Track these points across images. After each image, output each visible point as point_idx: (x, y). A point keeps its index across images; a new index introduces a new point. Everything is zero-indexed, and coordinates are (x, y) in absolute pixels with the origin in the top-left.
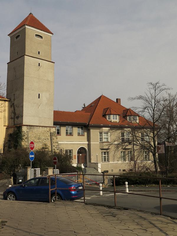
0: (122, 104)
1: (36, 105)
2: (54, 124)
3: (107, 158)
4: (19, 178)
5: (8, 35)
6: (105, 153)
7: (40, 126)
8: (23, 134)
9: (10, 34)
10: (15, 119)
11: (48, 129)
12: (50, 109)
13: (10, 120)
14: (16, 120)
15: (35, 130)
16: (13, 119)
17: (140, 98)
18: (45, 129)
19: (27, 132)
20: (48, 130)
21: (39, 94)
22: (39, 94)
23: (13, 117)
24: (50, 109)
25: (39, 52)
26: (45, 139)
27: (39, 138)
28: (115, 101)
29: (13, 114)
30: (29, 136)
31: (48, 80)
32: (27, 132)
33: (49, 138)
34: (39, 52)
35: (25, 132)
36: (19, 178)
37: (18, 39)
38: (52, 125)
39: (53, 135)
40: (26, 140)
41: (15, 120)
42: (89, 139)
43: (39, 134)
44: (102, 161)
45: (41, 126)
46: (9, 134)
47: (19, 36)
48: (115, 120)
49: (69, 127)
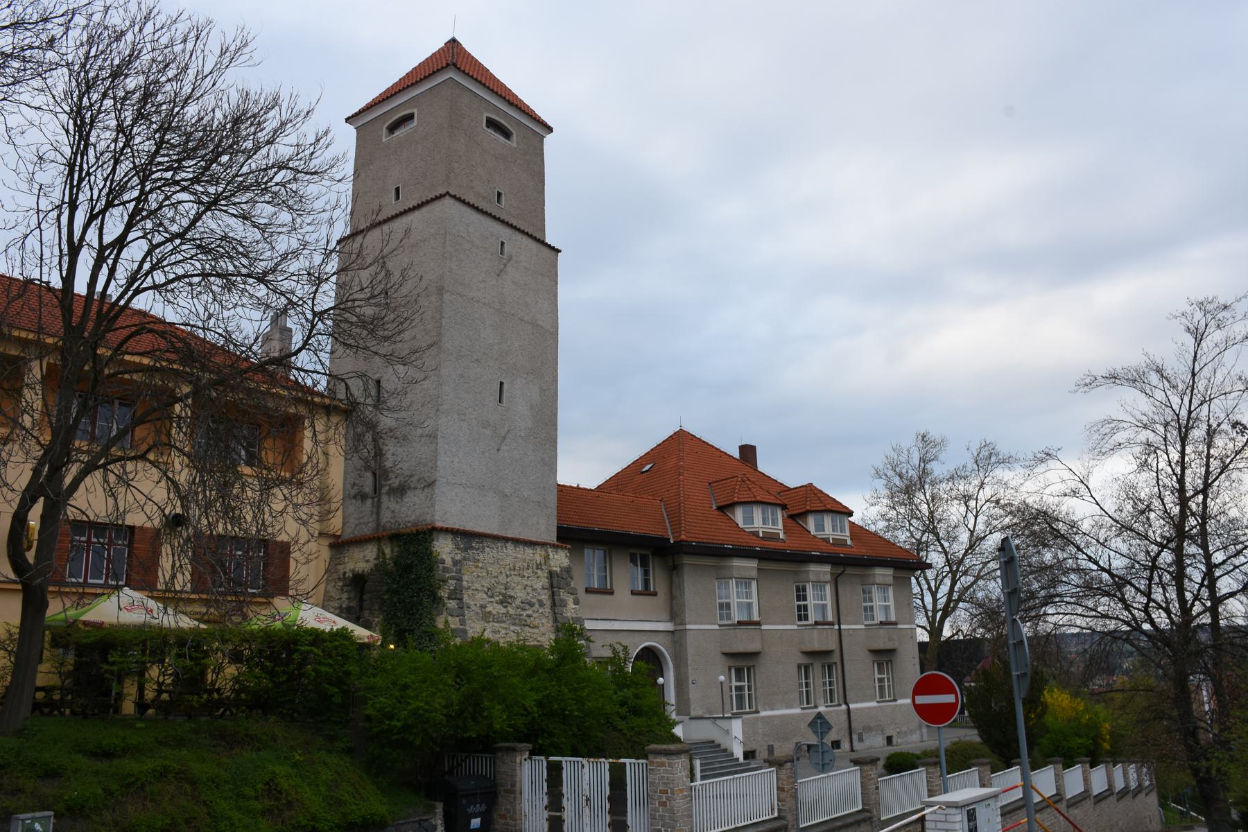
0: (762, 467)
1: (488, 432)
2: (558, 538)
3: (747, 692)
4: (471, 809)
5: (347, 120)
6: (739, 672)
7: (507, 539)
8: (439, 574)
9: (356, 115)
10: (385, 498)
11: (537, 555)
12: (543, 459)
13: (351, 509)
14: (388, 503)
15: (489, 554)
16: (369, 502)
17: (1135, 380)
18: (529, 551)
19: (455, 563)
20: (538, 559)
21: (502, 384)
22: (502, 384)
23: (368, 488)
24: (543, 459)
25: (499, 194)
26: (532, 605)
27: (504, 595)
28: (736, 455)
29: (369, 475)
30: (465, 583)
31: (535, 324)
32: (455, 563)
33: (545, 597)
34: (499, 194)
35: (449, 563)
36: (471, 809)
37: (401, 132)
38: (552, 537)
39: (562, 583)
40: (452, 604)
41: (384, 506)
42: (675, 614)
43: (502, 579)
44: (882, 695)
45: (510, 535)
46: (349, 575)
47: (410, 117)
48: (770, 528)
49: (588, 552)
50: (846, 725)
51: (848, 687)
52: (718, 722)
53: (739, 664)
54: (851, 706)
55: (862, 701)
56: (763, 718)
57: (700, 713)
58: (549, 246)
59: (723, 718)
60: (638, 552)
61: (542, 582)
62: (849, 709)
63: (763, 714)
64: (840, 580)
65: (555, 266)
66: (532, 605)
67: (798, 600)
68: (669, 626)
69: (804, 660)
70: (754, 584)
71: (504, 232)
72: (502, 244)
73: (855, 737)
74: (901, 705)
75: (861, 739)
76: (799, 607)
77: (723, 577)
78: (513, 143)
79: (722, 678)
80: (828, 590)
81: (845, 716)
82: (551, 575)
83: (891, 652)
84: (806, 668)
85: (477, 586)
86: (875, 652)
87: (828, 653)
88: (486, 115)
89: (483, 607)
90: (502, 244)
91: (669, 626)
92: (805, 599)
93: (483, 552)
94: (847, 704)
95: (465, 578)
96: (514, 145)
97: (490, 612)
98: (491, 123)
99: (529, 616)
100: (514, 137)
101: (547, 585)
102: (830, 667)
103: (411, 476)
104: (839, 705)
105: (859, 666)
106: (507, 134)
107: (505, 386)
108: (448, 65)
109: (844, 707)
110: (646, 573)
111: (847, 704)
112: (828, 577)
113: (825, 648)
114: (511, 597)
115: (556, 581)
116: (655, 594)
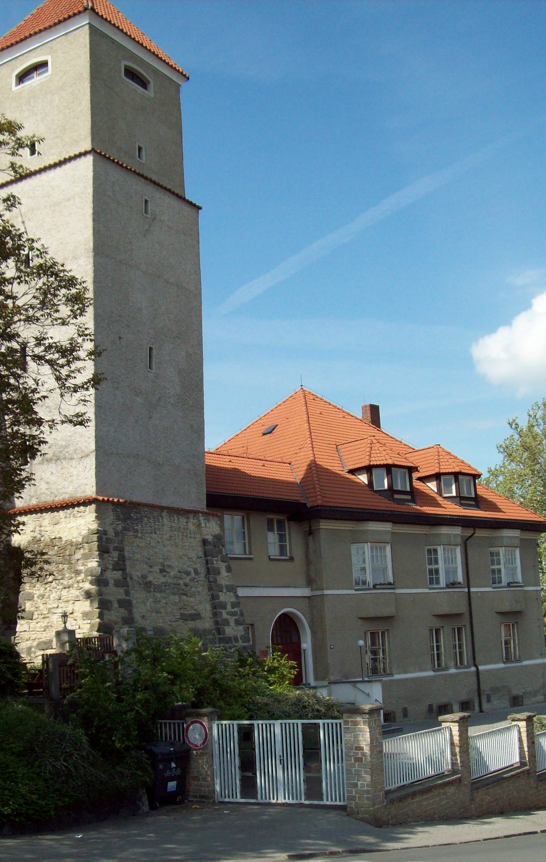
2: (209, 505)
12: (192, 426)
21: (151, 349)
22: (151, 349)
25: (140, 149)
32: (117, 534)
34: (140, 149)
38: (201, 505)
45: (164, 503)
50: (475, 687)
51: (477, 649)
52: (358, 685)
53: (373, 627)
54: (480, 668)
55: (490, 663)
56: (397, 680)
57: (338, 678)
58: (191, 203)
59: (363, 681)
60: (275, 517)
61: (196, 552)
62: (469, 592)
63: (397, 677)
64: (469, 542)
65: (197, 223)
66: (188, 574)
67: (430, 563)
68: (305, 592)
69: (437, 623)
70: (388, 548)
71: (149, 191)
72: (146, 202)
73: (484, 700)
74: (527, 666)
75: (489, 701)
76: (431, 571)
77: (358, 538)
78: (150, 93)
79: (361, 643)
80: (458, 551)
81: (475, 678)
82: (205, 542)
83: (518, 613)
84: (437, 631)
85: (138, 556)
86: (502, 614)
87: (458, 615)
88: (124, 63)
89: (144, 577)
90: (146, 202)
91: (305, 592)
92: (436, 562)
93: (141, 522)
94: (476, 666)
95: (127, 548)
96: (152, 95)
97: (150, 582)
98: (131, 74)
99: (186, 585)
100: (151, 86)
101: (201, 554)
102: (459, 630)
103: (66, 446)
104: (468, 667)
105: (487, 627)
106: (144, 84)
107: (154, 352)
108: (86, 9)
109: (473, 669)
110: (282, 538)
111: (476, 666)
112: (459, 540)
113: (455, 611)
114: (169, 566)
115: (212, 548)
116: (291, 559)
